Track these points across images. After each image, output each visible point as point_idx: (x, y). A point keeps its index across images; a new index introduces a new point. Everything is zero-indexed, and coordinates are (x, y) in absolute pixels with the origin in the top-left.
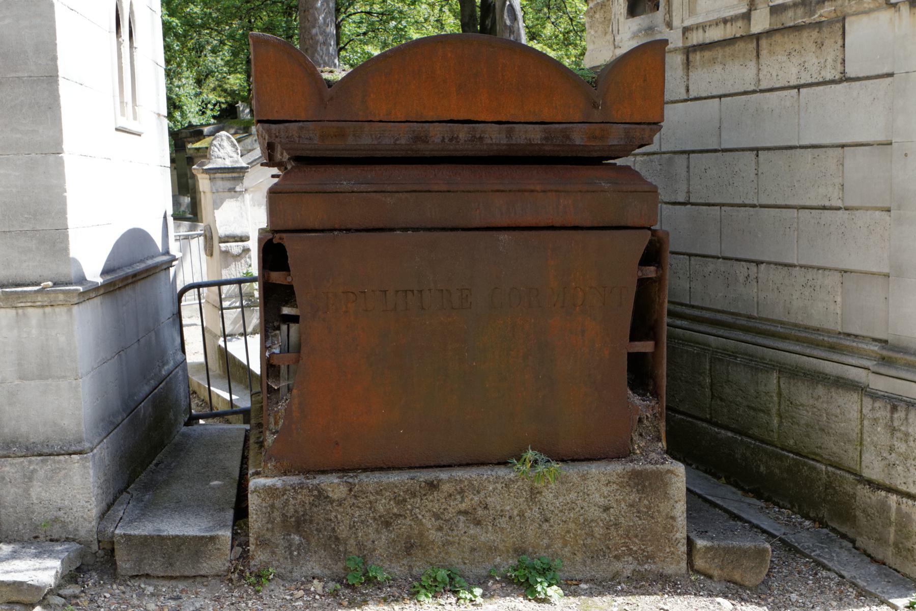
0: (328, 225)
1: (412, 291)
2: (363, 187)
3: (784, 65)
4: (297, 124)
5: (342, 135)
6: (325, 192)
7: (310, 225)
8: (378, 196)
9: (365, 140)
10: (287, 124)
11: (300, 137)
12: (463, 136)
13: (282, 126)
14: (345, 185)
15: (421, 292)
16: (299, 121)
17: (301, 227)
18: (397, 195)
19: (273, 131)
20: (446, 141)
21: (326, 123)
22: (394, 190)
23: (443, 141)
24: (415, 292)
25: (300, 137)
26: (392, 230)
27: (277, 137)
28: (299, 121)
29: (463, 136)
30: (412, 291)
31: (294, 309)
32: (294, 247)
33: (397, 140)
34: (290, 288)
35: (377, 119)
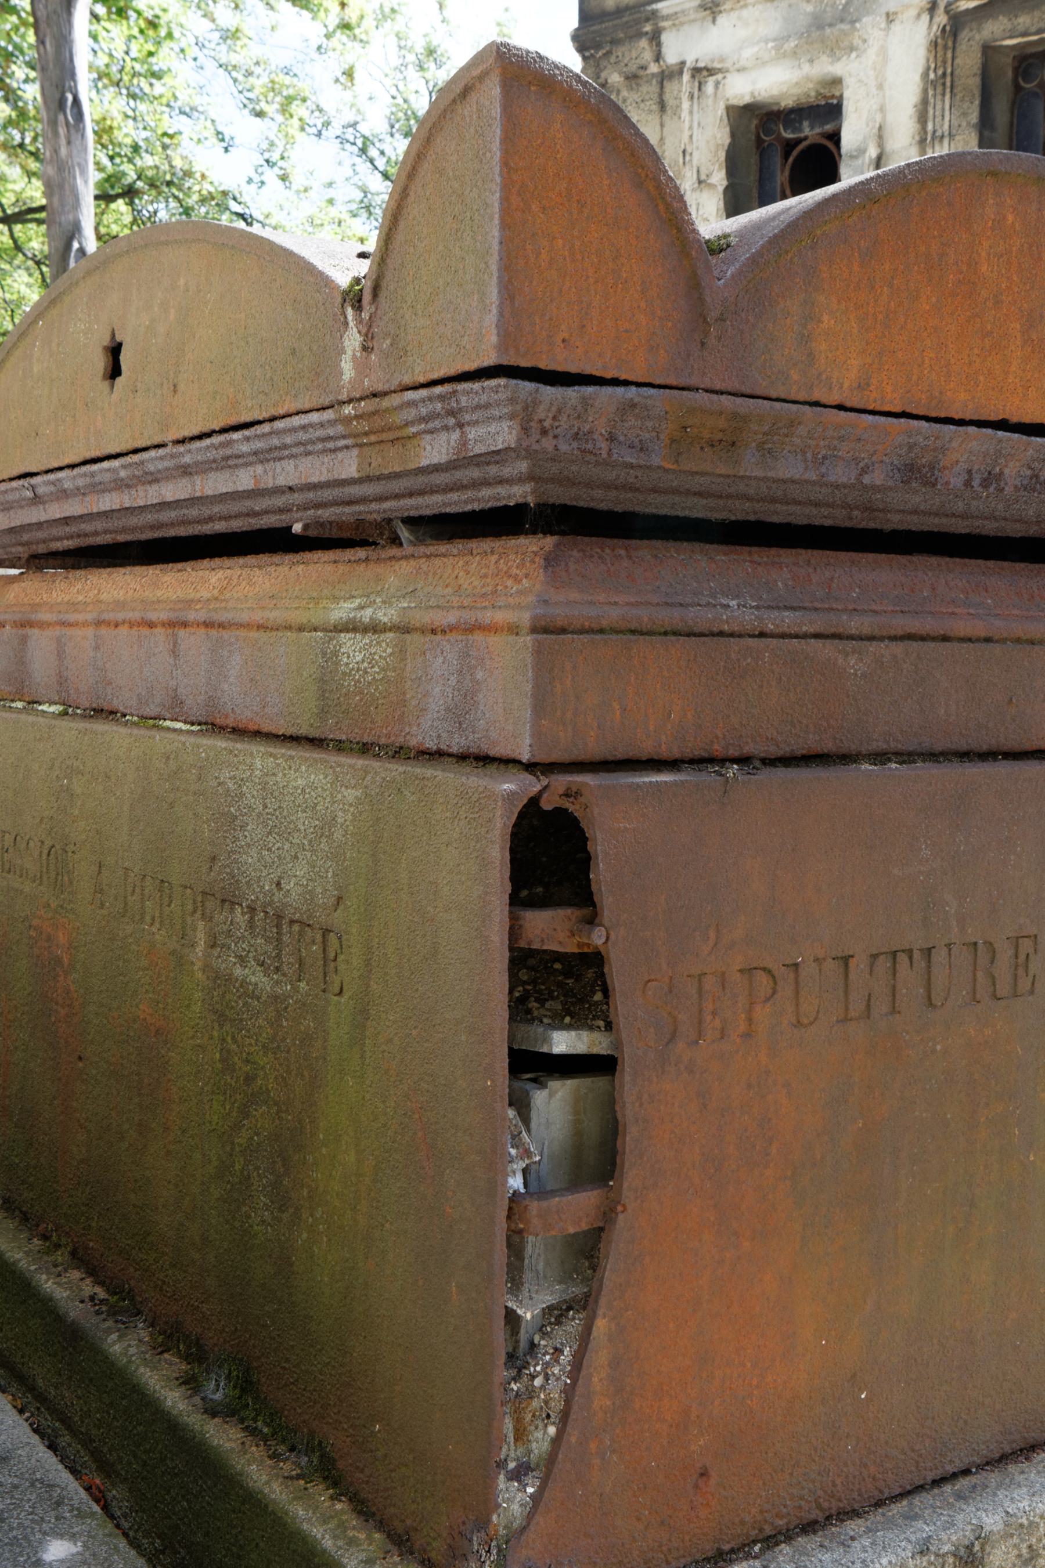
0: (694, 748)
1: (910, 952)
2: (788, 620)
3: (799, 457)
4: (620, 390)
5: (728, 445)
6: (690, 634)
7: (646, 748)
8: (826, 650)
9: (790, 473)
10: (590, 389)
11: (611, 438)
12: (1013, 472)
13: (572, 393)
14: (737, 612)
15: (928, 952)
16: (626, 383)
17: (620, 754)
18: (873, 647)
19: (541, 412)
20: (976, 483)
21: (701, 397)
22: (866, 630)
23: (968, 483)
24: (917, 955)
25: (611, 438)
26: (846, 758)
27: (544, 432)
28: (626, 383)
29: (1013, 472)
30: (910, 952)
31: (585, 1034)
32: (618, 822)
33: (864, 471)
34: (594, 960)
35: (835, 398)
